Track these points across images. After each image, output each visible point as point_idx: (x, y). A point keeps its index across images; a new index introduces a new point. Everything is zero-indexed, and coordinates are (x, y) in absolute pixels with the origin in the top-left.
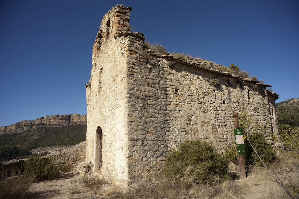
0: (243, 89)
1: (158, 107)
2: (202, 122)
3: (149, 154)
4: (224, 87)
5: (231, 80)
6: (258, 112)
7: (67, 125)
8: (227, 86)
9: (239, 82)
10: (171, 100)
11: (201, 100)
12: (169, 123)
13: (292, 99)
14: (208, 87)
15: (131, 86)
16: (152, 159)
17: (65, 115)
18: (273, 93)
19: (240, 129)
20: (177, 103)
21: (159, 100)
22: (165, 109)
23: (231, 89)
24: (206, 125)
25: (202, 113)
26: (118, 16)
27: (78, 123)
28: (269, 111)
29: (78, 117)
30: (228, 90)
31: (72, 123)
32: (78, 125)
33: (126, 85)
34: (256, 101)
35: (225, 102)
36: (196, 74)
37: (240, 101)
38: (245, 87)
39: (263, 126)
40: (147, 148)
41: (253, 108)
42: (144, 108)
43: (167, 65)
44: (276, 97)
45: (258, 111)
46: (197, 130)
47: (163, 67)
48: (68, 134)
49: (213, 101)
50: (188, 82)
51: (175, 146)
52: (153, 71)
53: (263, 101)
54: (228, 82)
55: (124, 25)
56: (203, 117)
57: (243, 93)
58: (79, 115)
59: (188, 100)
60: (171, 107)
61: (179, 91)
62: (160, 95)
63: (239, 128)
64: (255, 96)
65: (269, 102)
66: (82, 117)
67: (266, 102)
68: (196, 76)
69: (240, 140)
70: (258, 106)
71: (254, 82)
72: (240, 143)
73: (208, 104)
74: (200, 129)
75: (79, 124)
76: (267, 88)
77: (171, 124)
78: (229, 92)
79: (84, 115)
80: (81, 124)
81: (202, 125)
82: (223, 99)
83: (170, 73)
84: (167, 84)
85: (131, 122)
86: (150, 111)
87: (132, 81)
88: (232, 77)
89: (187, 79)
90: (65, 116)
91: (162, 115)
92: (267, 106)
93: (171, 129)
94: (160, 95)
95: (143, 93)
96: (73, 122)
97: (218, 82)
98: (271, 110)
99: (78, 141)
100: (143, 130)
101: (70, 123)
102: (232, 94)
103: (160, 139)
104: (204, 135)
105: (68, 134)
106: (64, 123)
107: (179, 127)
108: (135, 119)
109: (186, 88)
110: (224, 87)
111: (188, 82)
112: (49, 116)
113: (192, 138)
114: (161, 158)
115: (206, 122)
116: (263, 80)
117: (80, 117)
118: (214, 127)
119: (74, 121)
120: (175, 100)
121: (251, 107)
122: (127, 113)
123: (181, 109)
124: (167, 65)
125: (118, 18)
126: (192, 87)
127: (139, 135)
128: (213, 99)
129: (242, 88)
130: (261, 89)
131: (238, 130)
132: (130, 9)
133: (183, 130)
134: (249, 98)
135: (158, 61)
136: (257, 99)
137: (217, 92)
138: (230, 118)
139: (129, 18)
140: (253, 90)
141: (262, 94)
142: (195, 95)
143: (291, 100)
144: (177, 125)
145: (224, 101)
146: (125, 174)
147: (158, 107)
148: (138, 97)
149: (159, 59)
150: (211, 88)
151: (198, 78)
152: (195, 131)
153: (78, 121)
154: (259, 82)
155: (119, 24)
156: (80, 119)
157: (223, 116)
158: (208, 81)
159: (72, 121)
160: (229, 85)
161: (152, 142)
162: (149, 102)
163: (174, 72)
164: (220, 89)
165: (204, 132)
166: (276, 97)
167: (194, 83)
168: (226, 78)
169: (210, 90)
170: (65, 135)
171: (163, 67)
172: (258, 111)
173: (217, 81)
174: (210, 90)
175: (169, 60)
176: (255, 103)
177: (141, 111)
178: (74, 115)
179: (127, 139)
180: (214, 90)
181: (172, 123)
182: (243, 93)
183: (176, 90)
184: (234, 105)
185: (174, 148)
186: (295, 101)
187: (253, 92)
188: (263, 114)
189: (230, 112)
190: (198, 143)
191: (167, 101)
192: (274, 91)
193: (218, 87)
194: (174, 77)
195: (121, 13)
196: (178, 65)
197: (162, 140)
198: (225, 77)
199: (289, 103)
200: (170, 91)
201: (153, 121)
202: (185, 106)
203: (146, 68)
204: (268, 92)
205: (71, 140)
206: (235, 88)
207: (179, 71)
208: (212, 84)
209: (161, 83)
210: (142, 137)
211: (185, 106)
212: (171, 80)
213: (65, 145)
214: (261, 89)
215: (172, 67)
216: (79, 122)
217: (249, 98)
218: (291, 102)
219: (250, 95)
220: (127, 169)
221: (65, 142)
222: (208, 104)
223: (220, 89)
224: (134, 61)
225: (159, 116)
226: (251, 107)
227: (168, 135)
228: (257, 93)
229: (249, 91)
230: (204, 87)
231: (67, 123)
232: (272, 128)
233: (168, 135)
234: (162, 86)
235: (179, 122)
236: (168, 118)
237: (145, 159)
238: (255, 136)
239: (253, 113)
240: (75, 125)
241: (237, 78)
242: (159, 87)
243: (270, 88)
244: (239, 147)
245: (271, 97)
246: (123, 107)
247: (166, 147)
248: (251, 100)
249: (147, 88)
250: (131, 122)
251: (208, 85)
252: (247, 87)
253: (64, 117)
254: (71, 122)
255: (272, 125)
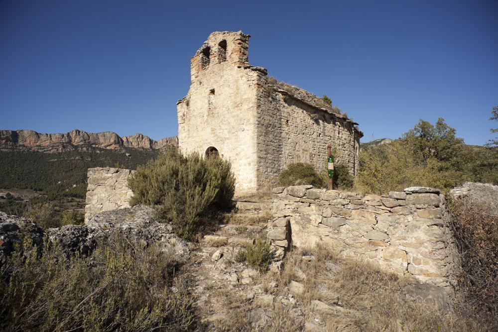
0: (335, 125)
1: (275, 134)
2: (303, 150)
3: (269, 170)
4: (321, 121)
5: (327, 116)
6: (345, 148)
7: (11, 150)
8: (323, 121)
9: (330, 117)
10: (284, 129)
11: (303, 132)
12: (282, 148)
13: (384, 139)
14: (309, 120)
15: (259, 115)
16: (271, 174)
17: (6, 131)
18: (359, 130)
19: (331, 158)
20: (288, 132)
21: (275, 128)
22: (279, 136)
23: (326, 123)
24: (305, 153)
25: (303, 143)
26: (239, 44)
27: (35, 149)
28: (354, 147)
29: (35, 137)
30: (323, 124)
31: (21, 148)
32: (34, 152)
33: (255, 114)
34: (344, 136)
35: (321, 135)
36: (301, 108)
37: (332, 135)
38: (336, 123)
39: (347, 161)
40: (268, 165)
41: (341, 143)
42: (267, 133)
43: (282, 98)
44: (361, 135)
45: (345, 146)
46: (299, 156)
47: (279, 101)
48: (12, 167)
49: (312, 133)
50: (295, 115)
51: (285, 166)
52: (273, 103)
53: (349, 138)
54: (324, 117)
55: (244, 54)
56: (304, 146)
57: (335, 129)
58: (37, 134)
59: (295, 130)
60: (283, 135)
61: (289, 122)
62: (276, 124)
63: (330, 157)
64: (343, 132)
65: (355, 139)
66: (43, 138)
67: (352, 139)
68: (301, 110)
69: (331, 166)
70: (345, 142)
71: (345, 119)
72: (331, 169)
73: (308, 136)
74: (301, 156)
75: (38, 152)
76: (355, 126)
77: (283, 149)
78: (324, 127)
79: (47, 135)
80: (40, 151)
81: (303, 153)
82: (319, 132)
83: (284, 106)
84: (281, 116)
85: (259, 144)
86: (270, 136)
87: (260, 111)
88: (328, 113)
89: (295, 112)
90: (5, 133)
91: (278, 141)
92: (353, 143)
93: (283, 152)
94: (276, 124)
95: (267, 122)
96: (24, 146)
97: (317, 117)
98: (356, 147)
99: (35, 182)
100: (266, 151)
101: (16, 146)
102: (326, 128)
103: (276, 159)
104: (304, 160)
105: (12, 167)
106: (4, 146)
107: (288, 152)
108: (261, 142)
109: (294, 120)
110: (321, 121)
111: (295, 115)
112: (69, 133)
113: (295, 161)
114: (275, 174)
115: (306, 151)
116: (352, 118)
117: (39, 137)
118: (311, 155)
119: (26, 144)
120: (286, 129)
121: (340, 142)
122: (256, 136)
123: (290, 137)
124: (282, 98)
125: (239, 45)
126: (298, 119)
127: (263, 154)
128: (312, 131)
129: (334, 123)
130: (349, 126)
131: (330, 159)
132: (249, 36)
133: (291, 154)
134: (339, 133)
135: (276, 95)
136: (345, 135)
137: (315, 125)
138: (323, 150)
139: (248, 46)
140: (343, 127)
141: (350, 130)
142: (300, 126)
143: (382, 140)
144: (286, 150)
145: (320, 134)
146: (252, 183)
147: (275, 134)
148: (263, 125)
149: (277, 93)
150: (312, 122)
151: (303, 112)
152: (298, 156)
153: (35, 145)
154: (348, 119)
155: (241, 52)
156: (39, 142)
157: (318, 147)
158: (309, 115)
159: (21, 143)
160: (325, 120)
161: (271, 161)
162: (269, 129)
163: (286, 105)
164: (318, 124)
165: (304, 158)
166: (361, 135)
167: (300, 116)
168: (323, 113)
169: (311, 123)
170: (7, 169)
171: (279, 101)
172: (345, 146)
173: (316, 116)
174: (311, 123)
175: (284, 95)
176: (343, 139)
177: (265, 136)
178: (25, 132)
179: (256, 157)
180: (313, 124)
181: (283, 148)
182: (335, 129)
183: (287, 121)
184: (327, 138)
185: (285, 167)
186: (387, 142)
187: (342, 128)
188: (348, 150)
189: (323, 145)
190: (302, 165)
191: (281, 130)
192: (360, 129)
193: (317, 121)
194: (288, 110)
195: (242, 41)
196: (291, 99)
197: (277, 161)
198: (322, 112)
199: (379, 144)
200: (284, 121)
201: (272, 145)
202: (292, 135)
203: (268, 101)
204: (355, 129)
205: (19, 179)
206: (329, 123)
207: (290, 105)
208: (312, 118)
209: (278, 114)
210: (265, 156)
211: (292, 135)
212: (284, 112)
213: (5, 188)
214: (349, 126)
215: (285, 101)
216: (37, 146)
217: (339, 133)
218: (382, 143)
219: (340, 130)
220: (256, 179)
221: (7, 183)
222: (308, 136)
223: (318, 124)
224: (261, 94)
225: (275, 142)
226: (340, 142)
227: (281, 157)
228: (346, 130)
229: (339, 126)
230: (306, 120)
231: (9, 147)
232: (354, 163)
233: (281, 157)
234: (278, 117)
235: (288, 148)
236: (281, 144)
237: (266, 173)
238: (341, 166)
239: (340, 147)
240: (28, 151)
241: (332, 114)
242: (277, 117)
243: (356, 126)
244: (330, 172)
245: (356, 134)
246: (250, 132)
247: (279, 166)
248: (340, 136)
249: (269, 118)
250: (259, 144)
251: (310, 118)
252: (338, 123)
253: (4, 135)
254: (20, 146)
255: (354, 161)
